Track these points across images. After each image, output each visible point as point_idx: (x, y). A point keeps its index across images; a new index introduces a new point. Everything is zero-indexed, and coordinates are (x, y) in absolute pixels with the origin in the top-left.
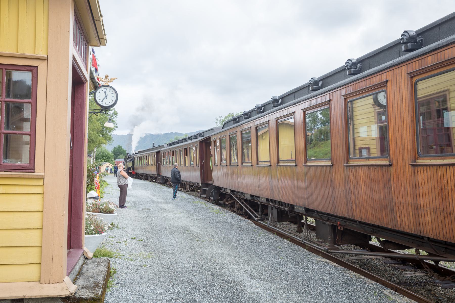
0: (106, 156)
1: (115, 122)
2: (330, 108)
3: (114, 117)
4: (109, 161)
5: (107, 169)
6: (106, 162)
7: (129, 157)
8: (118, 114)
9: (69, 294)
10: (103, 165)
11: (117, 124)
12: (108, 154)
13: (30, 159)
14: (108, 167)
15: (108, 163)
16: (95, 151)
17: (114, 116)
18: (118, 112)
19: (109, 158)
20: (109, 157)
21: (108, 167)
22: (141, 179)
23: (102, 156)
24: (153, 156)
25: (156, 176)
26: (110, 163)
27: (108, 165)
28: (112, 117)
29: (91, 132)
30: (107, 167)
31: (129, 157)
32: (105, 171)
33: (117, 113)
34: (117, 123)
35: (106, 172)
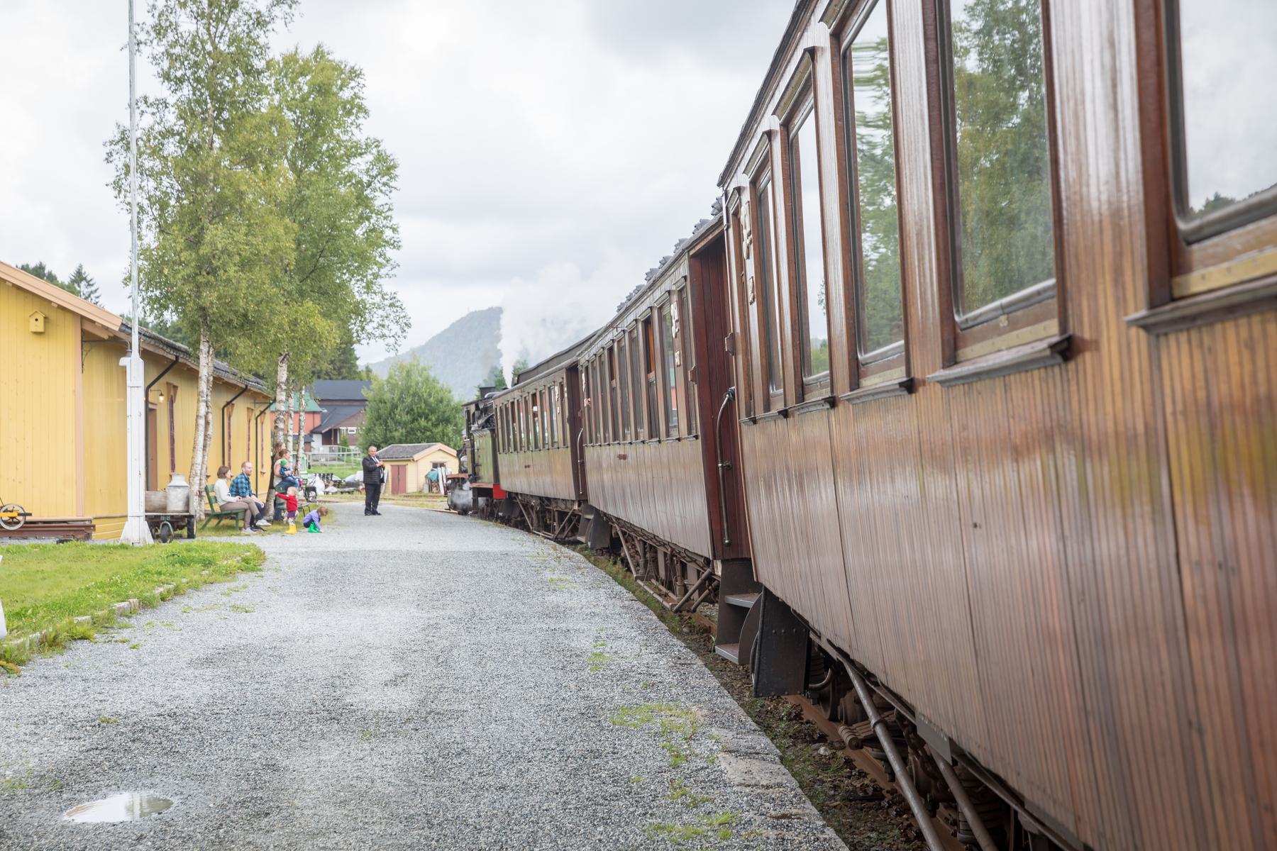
0: (433, 411)
1: (385, 218)
2: (1032, 834)
3: (374, 190)
4: (444, 434)
5: (435, 478)
6: (433, 439)
7: (481, 406)
8: (397, 172)
9: (919, 710)
10: (416, 457)
11: (394, 230)
12: (441, 401)
13: (582, 456)
14: (442, 465)
15: (439, 445)
16: (284, 379)
17: (378, 185)
18: (399, 161)
19: (447, 421)
20: (447, 415)
21: (442, 465)
22: (529, 531)
23: (412, 410)
24: (557, 389)
25: (576, 507)
26: (448, 445)
27: (439, 458)
28: (368, 191)
29: (231, 273)
30: (435, 465)
31: (481, 406)
32: (426, 487)
33: (394, 167)
34: (394, 222)
35: (430, 490)
